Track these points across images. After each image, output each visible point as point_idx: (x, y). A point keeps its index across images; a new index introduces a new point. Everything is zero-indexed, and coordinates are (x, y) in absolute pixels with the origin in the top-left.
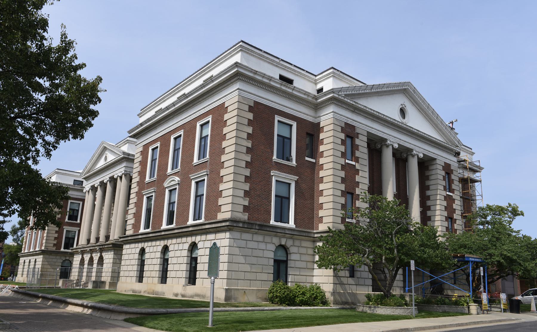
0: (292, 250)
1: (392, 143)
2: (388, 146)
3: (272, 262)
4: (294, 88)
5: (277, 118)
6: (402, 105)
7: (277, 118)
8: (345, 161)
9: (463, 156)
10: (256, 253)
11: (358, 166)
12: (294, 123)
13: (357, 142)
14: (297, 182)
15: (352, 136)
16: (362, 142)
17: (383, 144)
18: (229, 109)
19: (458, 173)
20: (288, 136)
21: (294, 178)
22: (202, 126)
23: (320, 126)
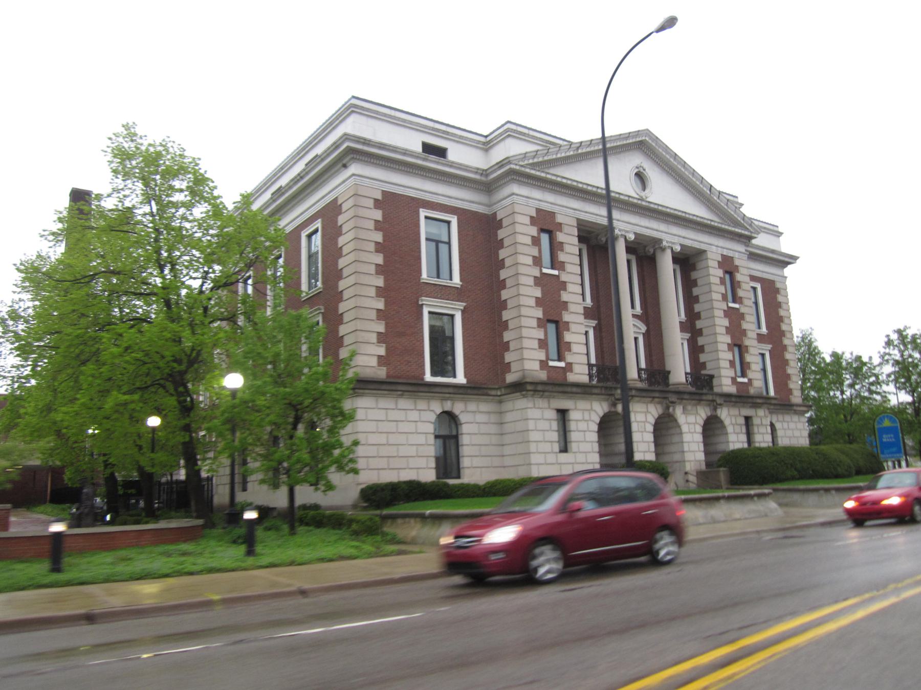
0: (463, 418)
1: (670, 245)
2: (663, 249)
3: (431, 439)
4: (452, 165)
5: (423, 213)
6: (637, 168)
7: (423, 213)
8: (727, 305)
9: (762, 241)
10: (403, 427)
11: (743, 310)
12: (454, 218)
13: (560, 237)
14: (464, 312)
15: (551, 229)
16: (569, 239)
17: (657, 247)
18: (344, 208)
19: (746, 269)
20: (446, 239)
21: (592, 323)
22: (309, 236)
23: (496, 219)
